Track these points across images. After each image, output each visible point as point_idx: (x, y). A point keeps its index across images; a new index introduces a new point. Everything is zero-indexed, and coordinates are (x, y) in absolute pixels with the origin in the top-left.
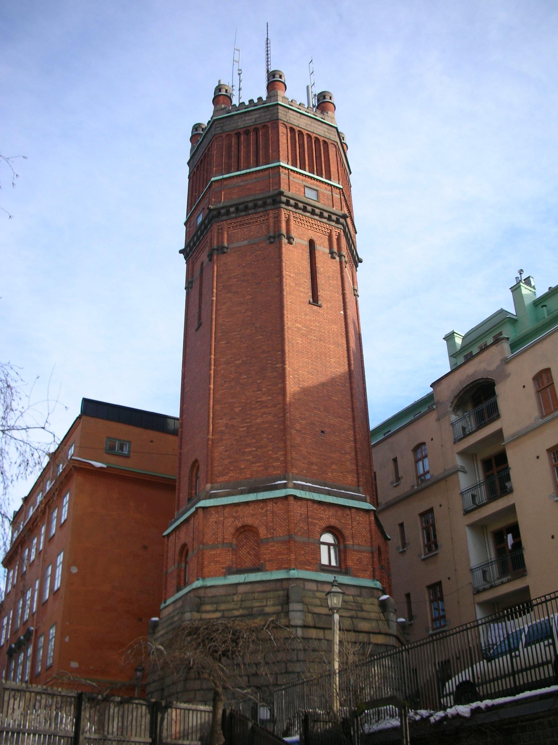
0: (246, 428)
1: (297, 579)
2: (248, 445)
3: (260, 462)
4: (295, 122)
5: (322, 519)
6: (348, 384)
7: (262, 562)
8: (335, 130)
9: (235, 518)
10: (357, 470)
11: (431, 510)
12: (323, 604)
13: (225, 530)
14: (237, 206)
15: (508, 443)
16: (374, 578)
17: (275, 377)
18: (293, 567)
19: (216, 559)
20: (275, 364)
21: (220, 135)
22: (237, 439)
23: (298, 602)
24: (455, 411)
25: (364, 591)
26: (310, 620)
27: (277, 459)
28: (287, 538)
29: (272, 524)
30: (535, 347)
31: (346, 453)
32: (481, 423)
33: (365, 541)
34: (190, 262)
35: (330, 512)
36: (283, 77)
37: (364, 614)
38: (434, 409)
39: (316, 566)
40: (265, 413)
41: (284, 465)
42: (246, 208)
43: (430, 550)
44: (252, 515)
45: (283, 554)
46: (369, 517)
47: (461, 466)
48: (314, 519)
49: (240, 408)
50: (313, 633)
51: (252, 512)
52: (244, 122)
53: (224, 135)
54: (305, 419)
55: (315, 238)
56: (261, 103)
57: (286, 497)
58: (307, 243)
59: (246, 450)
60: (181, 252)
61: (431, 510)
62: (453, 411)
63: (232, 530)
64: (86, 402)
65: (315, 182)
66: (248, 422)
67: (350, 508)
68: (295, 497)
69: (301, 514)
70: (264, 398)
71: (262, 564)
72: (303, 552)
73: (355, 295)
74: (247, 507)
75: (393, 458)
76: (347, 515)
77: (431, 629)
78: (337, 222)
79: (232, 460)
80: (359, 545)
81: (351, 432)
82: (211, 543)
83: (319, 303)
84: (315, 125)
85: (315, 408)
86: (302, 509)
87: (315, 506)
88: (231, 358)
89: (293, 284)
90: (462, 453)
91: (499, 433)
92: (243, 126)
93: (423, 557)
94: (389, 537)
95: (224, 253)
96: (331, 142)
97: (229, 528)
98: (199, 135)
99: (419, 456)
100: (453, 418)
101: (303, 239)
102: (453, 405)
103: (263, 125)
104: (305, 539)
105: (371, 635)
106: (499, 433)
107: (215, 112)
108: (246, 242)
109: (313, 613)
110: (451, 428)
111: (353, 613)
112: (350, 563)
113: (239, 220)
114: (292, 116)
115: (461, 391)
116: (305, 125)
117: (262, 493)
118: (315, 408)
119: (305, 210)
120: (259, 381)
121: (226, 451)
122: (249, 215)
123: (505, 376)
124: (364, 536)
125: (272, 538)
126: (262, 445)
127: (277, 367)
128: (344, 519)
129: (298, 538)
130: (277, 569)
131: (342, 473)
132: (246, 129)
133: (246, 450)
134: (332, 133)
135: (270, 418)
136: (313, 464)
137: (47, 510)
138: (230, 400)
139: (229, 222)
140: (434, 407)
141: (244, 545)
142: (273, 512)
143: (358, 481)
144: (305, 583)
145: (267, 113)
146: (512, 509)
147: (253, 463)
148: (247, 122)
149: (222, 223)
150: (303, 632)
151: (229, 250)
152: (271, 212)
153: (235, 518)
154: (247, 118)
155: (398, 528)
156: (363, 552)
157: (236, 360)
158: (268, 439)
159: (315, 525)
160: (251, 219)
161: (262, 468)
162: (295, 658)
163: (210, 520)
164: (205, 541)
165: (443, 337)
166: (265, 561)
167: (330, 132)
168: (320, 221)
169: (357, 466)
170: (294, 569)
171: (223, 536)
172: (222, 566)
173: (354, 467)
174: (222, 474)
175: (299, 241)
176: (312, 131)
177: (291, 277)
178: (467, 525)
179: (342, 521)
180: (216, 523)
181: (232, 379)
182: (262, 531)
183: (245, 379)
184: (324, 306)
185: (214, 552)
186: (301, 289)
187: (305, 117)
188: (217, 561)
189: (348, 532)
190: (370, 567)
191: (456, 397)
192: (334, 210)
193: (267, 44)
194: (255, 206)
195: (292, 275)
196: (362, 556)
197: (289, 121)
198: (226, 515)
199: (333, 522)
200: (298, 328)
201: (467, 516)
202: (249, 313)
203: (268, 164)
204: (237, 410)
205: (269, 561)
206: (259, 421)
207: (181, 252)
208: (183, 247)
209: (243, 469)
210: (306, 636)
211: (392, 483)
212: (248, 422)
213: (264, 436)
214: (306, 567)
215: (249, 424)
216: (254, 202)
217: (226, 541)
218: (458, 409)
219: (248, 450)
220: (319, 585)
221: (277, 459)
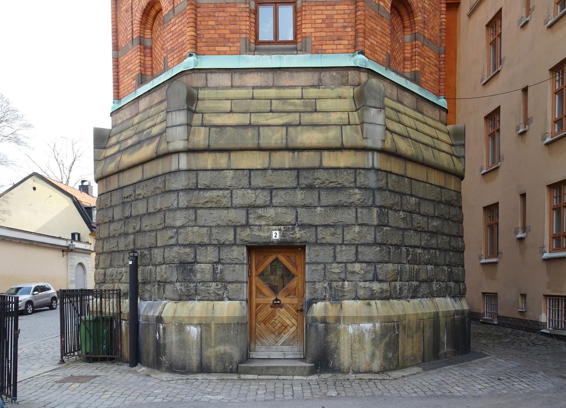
12: (234, 109)
16: (355, 49)
23: (180, 110)
25: (326, 76)
26: (200, 138)
37: (317, 118)
39: (238, 44)
50: (208, 161)
72: (214, 23)
77: (547, 249)
105: (326, 154)
109: (211, 126)
111: (293, 118)
141: (159, 36)
144: (209, 75)
150: (188, 162)
162: (175, 204)
185: (127, 58)
190: (349, 29)
210: (194, 167)
214: (218, 49)
220: (237, 76)
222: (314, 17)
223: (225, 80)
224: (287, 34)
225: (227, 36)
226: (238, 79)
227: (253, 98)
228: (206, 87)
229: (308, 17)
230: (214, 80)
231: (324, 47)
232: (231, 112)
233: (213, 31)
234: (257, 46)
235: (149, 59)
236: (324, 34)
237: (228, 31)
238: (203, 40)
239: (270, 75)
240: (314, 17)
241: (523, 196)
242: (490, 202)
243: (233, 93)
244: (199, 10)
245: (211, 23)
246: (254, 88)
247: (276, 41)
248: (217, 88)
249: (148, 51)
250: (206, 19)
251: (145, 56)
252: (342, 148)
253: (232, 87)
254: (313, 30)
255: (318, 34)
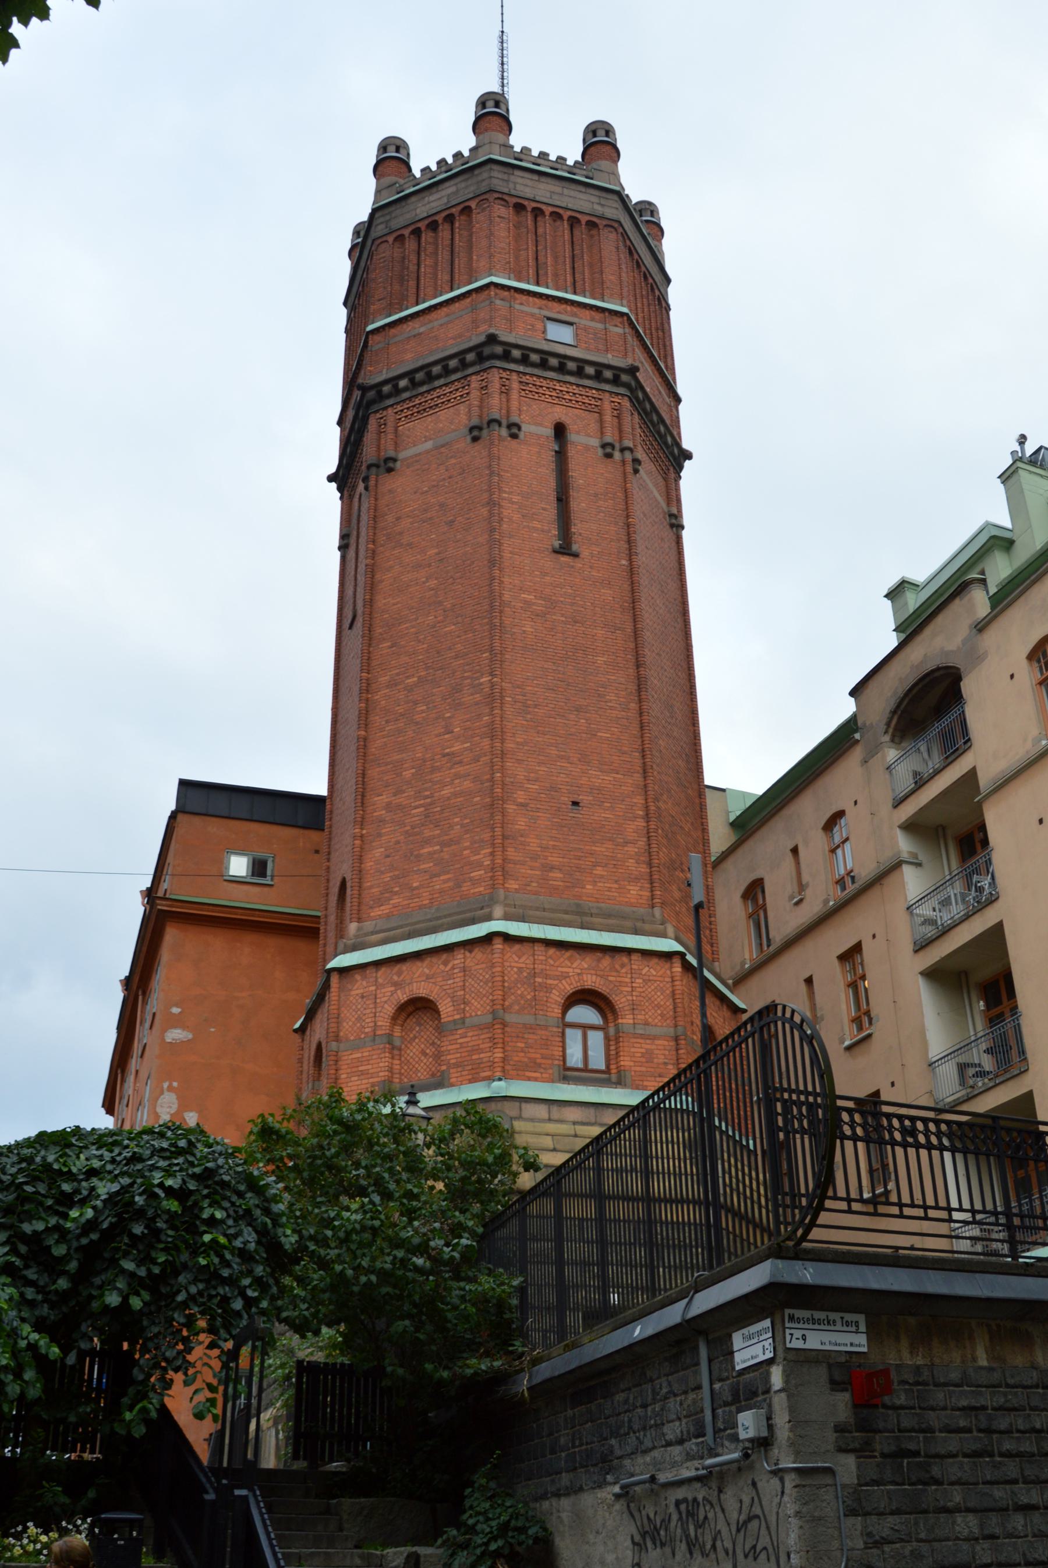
0: (422, 809)
1: (505, 1098)
2: (428, 841)
3: (448, 873)
4: (528, 192)
5: (565, 976)
6: (633, 705)
7: (444, 1068)
8: (616, 197)
9: (396, 984)
10: (651, 875)
11: (857, 948)
12: (558, 1147)
13: (378, 1010)
14: (410, 374)
15: (988, 796)
17: (477, 704)
18: (498, 1074)
19: (361, 1068)
20: (478, 678)
21: (384, 239)
22: (407, 832)
24: (897, 740)
27: (479, 865)
28: (489, 1018)
29: (462, 993)
30: (1027, 593)
31: (627, 843)
32: (949, 760)
33: (662, 1015)
34: (346, 492)
35: (584, 962)
36: (502, 106)
38: (857, 741)
39: (550, 1071)
40: (457, 776)
41: (490, 874)
42: (430, 378)
43: (860, 1028)
44: (428, 977)
45: (481, 1051)
46: (671, 967)
47: (910, 853)
48: (547, 977)
49: (414, 770)
51: (427, 971)
52: (428, 206)
53: (391, 239)
54: (536, 780)
55: (566, 420)
56: (459, 162)
57: (488, 939)
58: (550, 432)
59: (422, 851)
60: (330, 479)
61: (857, 948)
62: (892, 740)
63: (390, 1009)
64: (185, 785)
65: (569, 308)
66: (427, 797)
67: (629, 951)
68: (506, 937)
69: (520, 969)
70: (457, 747)
71: (443, 1072)
73: (672, 526)
74: (419, 964)
75: (792, 847)
76: (623, 966)
78: (616, 381)
79: (397, 873)
80: (647, 1024)
81: (639, 800)
82: (352, 1038)
83: (575, 548)
84: (572, 193)
85: (562, 757)
86: (522, 960)
87: (552, 951)
88: (398, 674)
89: (516, 517)
90: (911, 827)
91: (971, 775)
92: (425, 215)
93: (847, 1043)
94: (742, 1006)
95: (390, 470)
96: (605, 222)
97: (386, 1006)
98: (365, 244)
99: (837, 839)
100: (892, 754)
101: (541, 425)
102: (891, 730)
103: (462, 206)
104: (529, 1019)
106: (971, 775)
107: (378, 192)
108: (429, 445)
110: (887, 776)
112: (626, 1062)
113: (417, 402)
114: (520, 180)
115: (902, 700)
116: (548, 195)
117: (446, 933)
118: (562, 757)
119: (543, 365)
120: (448, 715)
121: (388, 856)
122: (434, 389)
123: (977, 658)
124: (658, 1006)
125: (463, 1020)
126: (451, 840)
127: (481, 684)
128: (614, 974)
129: (509, 1018)
130: (470, 1081)
131: (616, 882)
132: (430, 220)
133: (422, 851)
134: (610, 203)
135: (467, 784)
136: (552, 868)
137: (140, 998)
138: (397, 757)
139: (399, 408)
140: (857, 736)
141: (415, 1037)
142: (464, 970)
143: (653, 897)
144: (524, 1105)
145: (469, 182)
146: (997, 932)
147: (435, 876)
148: (433, 205)
149: (385, 413)
151: (398, 464)
152: (474, 377)
153: (396, 984)
154: (432, 198)
155: (803, 987)
156: (654, 1038)
157: (408, 677)
158: (462, 826)
159: (548, 989)
160: (438, 397)
161: (450, 884)
163: (353, 993)
164: (341, 1034)
165: (885, 592)
166: (449, 1066)
167: (603, 202)
168: (578, 385)
169: (650, 865)
170: (500, 1079)
171: (375, 1022)
172: (371, 1080)
173: (644, 869)
174: (379, 902)
175: (533, 429)
176: (564, 205)
177: (513, 503)
178: (921, 973)
179: (611, 978)
180: (363, 997)
181: (402, 715)
182: (446, 1008)
183: (423, 712)
184: (585, 553)
185: (359, 1055)
186: (536, 524)
187: (549, 180)
188: (362, 1073)
189: (624, 1000)
190: (670, 1067)
191: (894, 712)
192: (610, 359)
193: (502, 42)
194: (447, 371)
195: (516, 498)
196: (654, 1047)
197: (513, 192)
198: (380, 981)
199: (590, 981)
200: (526, 602)
201: (921, 954)
202: (433, 583)
203: (471, 283)
204: (407, 774)
205: (457, 1065)
206: (446, 792)
207: (330, 479)
208: (332, 468)
209: (416, 888)
211: (791, 898)
212: (427, 797)
213: (456, 820)
215: (429, 800)
216: (581, 364)
217: (379, 1032)
218: (903, 738)
219: (426, 850)
220: (555, 1109)
221: (479, 865)
222: (633, 1050)
223: (541, 1111)
224: (597, 1061)
225: (538, 1061)
226: (555, 1110)
227: (576, 1136)
228: (520, 1118)
229: (626, 1049)
230: (529, 1110)
231: (645, 1083)
232: (554, 1150)
233: (522, 1054)
234: (567, 1075)
235: (398, 1062)
236: (644, 1069)
237: (538, 1056)
238: (511, 1063)
239: (592, 1111)
240: (633, 1050)
241: (565, 549)
242: (807, 975)
243: (552, 1127)
244: (507, 1029)
245: (519, 1044)
246: (574, 1123)
247: (586, 1069)
248: (532, 1120)
249: (396, 1052)
250: (514, 1039)
251: (393, 1058)
252: (681, 1201)
253: (550, 1120)
254: (632, 1064)
255: (638, 1069)
